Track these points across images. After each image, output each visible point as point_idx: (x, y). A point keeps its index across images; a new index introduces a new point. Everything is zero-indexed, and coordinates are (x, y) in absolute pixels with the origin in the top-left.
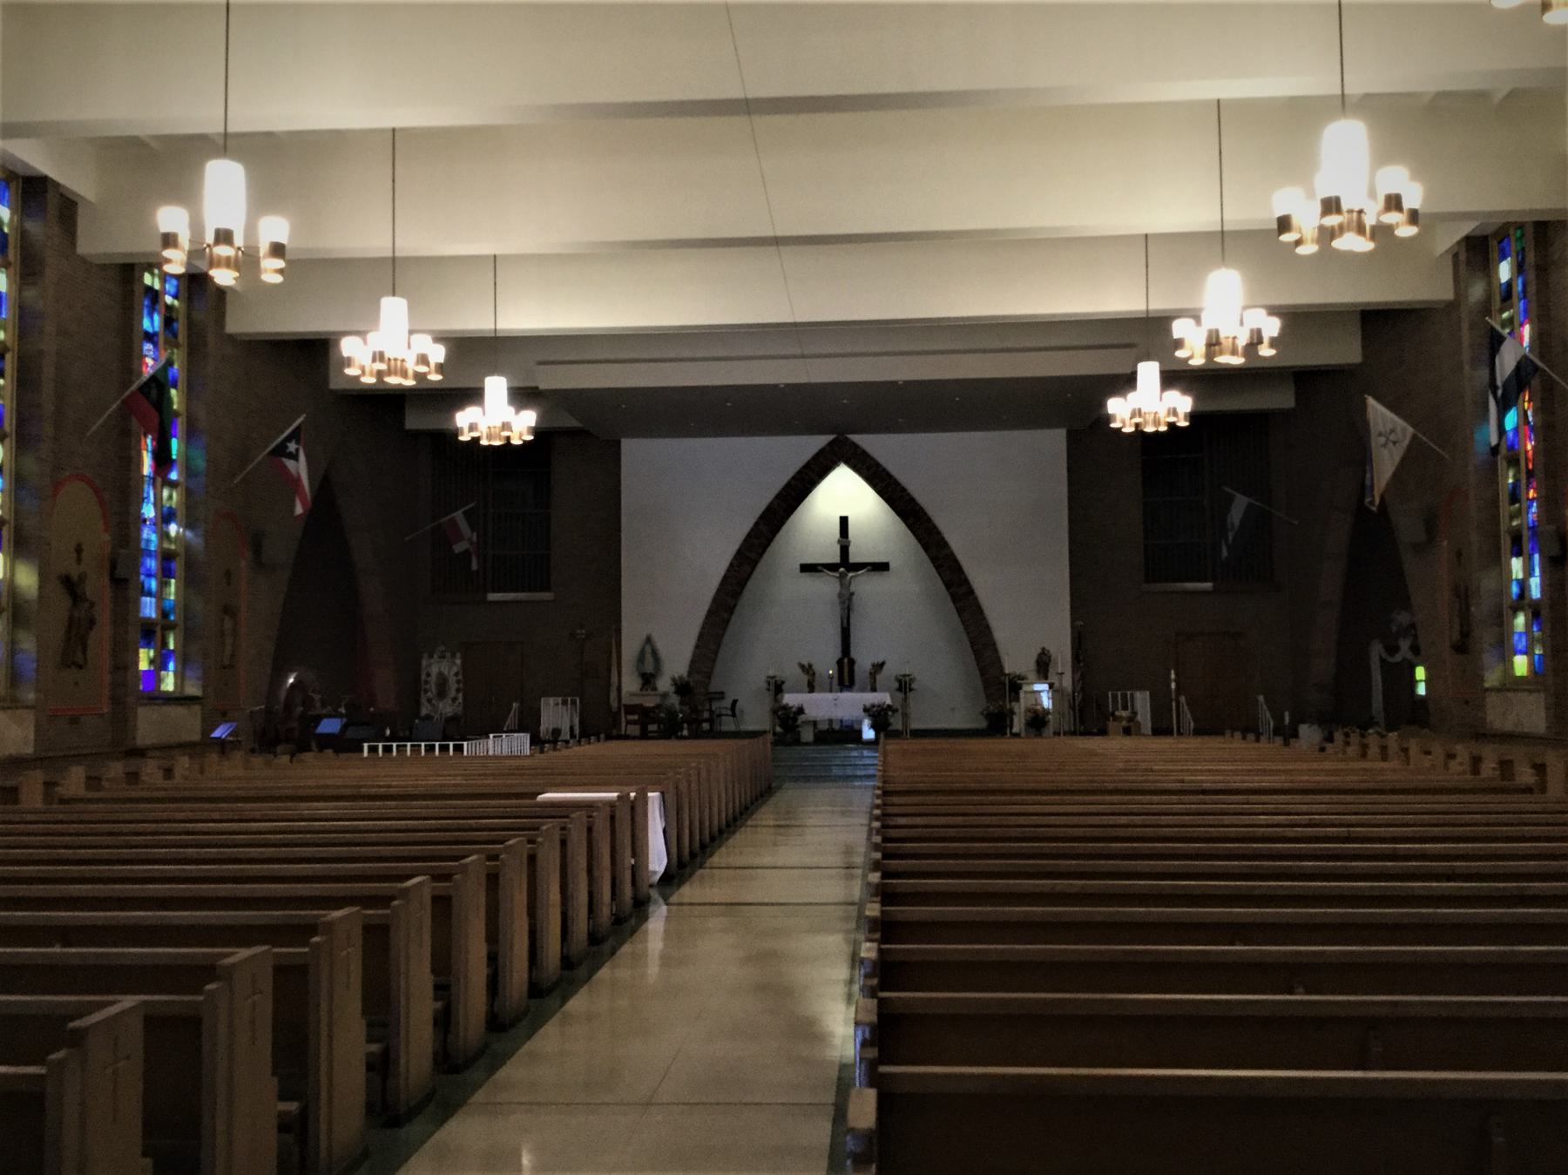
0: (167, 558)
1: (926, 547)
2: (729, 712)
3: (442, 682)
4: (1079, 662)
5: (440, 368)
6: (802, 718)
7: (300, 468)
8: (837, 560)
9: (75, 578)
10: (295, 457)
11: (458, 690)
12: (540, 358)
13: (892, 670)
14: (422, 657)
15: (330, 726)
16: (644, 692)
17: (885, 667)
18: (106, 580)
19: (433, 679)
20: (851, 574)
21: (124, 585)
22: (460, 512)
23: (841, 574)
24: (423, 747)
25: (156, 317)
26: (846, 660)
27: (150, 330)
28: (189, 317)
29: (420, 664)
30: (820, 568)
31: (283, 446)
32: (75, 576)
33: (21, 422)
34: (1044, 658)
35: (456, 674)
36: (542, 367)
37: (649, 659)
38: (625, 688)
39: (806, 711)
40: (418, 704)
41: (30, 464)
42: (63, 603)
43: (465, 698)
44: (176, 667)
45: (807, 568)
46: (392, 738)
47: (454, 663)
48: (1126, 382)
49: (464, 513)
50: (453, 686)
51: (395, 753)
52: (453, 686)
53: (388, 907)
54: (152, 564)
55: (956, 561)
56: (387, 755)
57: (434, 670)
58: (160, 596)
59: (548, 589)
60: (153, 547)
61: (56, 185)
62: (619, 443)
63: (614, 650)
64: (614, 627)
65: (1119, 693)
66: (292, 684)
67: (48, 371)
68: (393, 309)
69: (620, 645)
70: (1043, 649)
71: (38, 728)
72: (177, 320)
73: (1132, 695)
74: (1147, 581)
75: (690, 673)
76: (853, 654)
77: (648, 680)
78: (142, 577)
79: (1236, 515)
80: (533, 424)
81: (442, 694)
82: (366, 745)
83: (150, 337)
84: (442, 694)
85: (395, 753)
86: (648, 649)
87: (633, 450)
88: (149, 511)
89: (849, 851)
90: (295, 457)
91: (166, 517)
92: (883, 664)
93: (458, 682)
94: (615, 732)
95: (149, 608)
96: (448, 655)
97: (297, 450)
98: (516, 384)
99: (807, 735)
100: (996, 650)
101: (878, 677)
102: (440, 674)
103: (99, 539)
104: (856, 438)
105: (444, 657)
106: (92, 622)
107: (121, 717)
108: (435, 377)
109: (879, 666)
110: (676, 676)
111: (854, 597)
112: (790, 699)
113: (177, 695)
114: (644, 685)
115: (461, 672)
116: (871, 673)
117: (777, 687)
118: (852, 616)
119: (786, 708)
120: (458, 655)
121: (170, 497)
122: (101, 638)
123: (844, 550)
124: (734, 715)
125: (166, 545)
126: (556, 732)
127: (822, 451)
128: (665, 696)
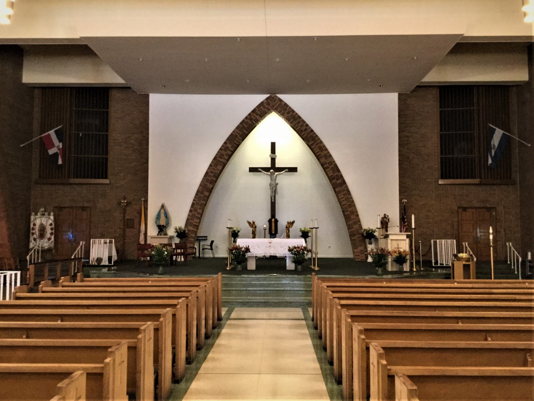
1: (318, 157)
2: (209, 247)
3: (42, 229)
4: (404, 223)
6: (248, 255)
8: (269, 165)
11: (51, 234)
13: (299, 226)
16: (159, 236)
17: (294, 224)
19: (37, 227)
20: (276, 173)
23: (271, 173)
26: (273, 220)
29: (30, 219)
30: (260, 170)
34: (385, 219)
35: (51, 225)
37: (162, 215)
38: (149, 234)
39: (251, 251)
40: (29, 242)
45: (253, 170)
47: (49, 218)
49: (56, 132)
50: (49, 231)
52: (49, 231)
55: (336, 166)
57: (38, 222)
62: (148, 96)
64: (143, 199)
65: (438, 241)
69: (147, 209)
70: (385, 215)
73: (435, 243)
74: (442, 178)
75: (187, 225)
76: (277, 217)
77: (162, 229)
79: (496, 140)
81: (42, 235)
84: (42, 235)
86: (162, 211)
89: (267, 254)
92: (293, 222)
93: (52, 229)
96: (46, 213)
99: (252, 265)
100: (357, 215)
101: (290, 229)
104: (281, 96)
105: (43, 215)
109: (291, 224)
110: (178, 228)
111: (278, 186)
112: (241, 242)
114: (159, 232)
116: (287, 227)
117: (235, 235)
118: (276, 196)
119: (238, 249)
120: (52, 214)
123: (273, 160)
124: (212, 249)
126: (99, 260)
127: (262, 104)
128: (171, 238)
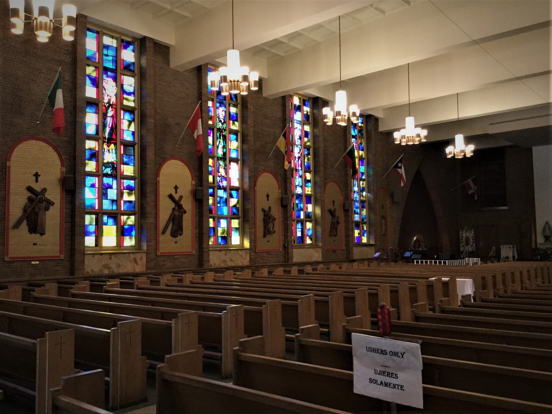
0: (362, 202)
3: (467, 240)
5: (426, 137)
7: (402, 171)
9: (333, 210)
10: (400, 168)
11: (473, 242)
12: (490, 123)
14: (460, 231)
15: (407, 254)
16: (546, 243)
18: (342, 210)
19: (464, 239)
21: (348, 211)
22: (470, 179)
24: (424, 262)
25: (356, 130)
27: (354, 134)
28: (367, 130)
31: (397, 165)
32: (332, 210)
33: (315, 167)
35: (472, 237)
36: (491, 126)
40: (459, 248)
41: (318, 179)
42: (329, 217)
43: (476, 245)
44: (367, 235)
46: (437, 259)
47: (471, 233)
48: (451, 142)
51: (442, 264)
53: (297, 301)
54: (357, 204)
56: (440, 264)
58: (360, 214)
59: (506, 206)
60: (358, 199)
61: (321, 98)
62: (532, 148)
63: (533, 229)
66: (415, 240)
67: (321, 152)
68: (410, 121)
71: (322, 253)
72: (363, 130)
78: (355, 209)
80: (473, 149)
82: (415, 261)
83: (354, 137)
85: (442, 264)
86: (547, 226)
87: (537, 151)
88: (356, 189)
90: (400, 168)
91: (362, 190)
93: (473, 239)
94: (535, 258)
95: (357, 218)
97: (401, 166)
98: (465, 136)
102: (467, 237)
103: (339, 199)
105: (467, 231)
106: (338, 223)
107: (349, 251)
108: (424, 141)
113: (368, 244)
114: (545, 240)
115: (474, 236)
120: (472, 230)
121: (363, 184)
122: (341, 227)
125: (362, 198)
126: (507, 258)
